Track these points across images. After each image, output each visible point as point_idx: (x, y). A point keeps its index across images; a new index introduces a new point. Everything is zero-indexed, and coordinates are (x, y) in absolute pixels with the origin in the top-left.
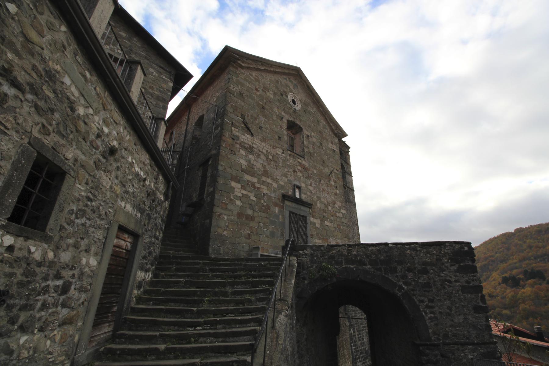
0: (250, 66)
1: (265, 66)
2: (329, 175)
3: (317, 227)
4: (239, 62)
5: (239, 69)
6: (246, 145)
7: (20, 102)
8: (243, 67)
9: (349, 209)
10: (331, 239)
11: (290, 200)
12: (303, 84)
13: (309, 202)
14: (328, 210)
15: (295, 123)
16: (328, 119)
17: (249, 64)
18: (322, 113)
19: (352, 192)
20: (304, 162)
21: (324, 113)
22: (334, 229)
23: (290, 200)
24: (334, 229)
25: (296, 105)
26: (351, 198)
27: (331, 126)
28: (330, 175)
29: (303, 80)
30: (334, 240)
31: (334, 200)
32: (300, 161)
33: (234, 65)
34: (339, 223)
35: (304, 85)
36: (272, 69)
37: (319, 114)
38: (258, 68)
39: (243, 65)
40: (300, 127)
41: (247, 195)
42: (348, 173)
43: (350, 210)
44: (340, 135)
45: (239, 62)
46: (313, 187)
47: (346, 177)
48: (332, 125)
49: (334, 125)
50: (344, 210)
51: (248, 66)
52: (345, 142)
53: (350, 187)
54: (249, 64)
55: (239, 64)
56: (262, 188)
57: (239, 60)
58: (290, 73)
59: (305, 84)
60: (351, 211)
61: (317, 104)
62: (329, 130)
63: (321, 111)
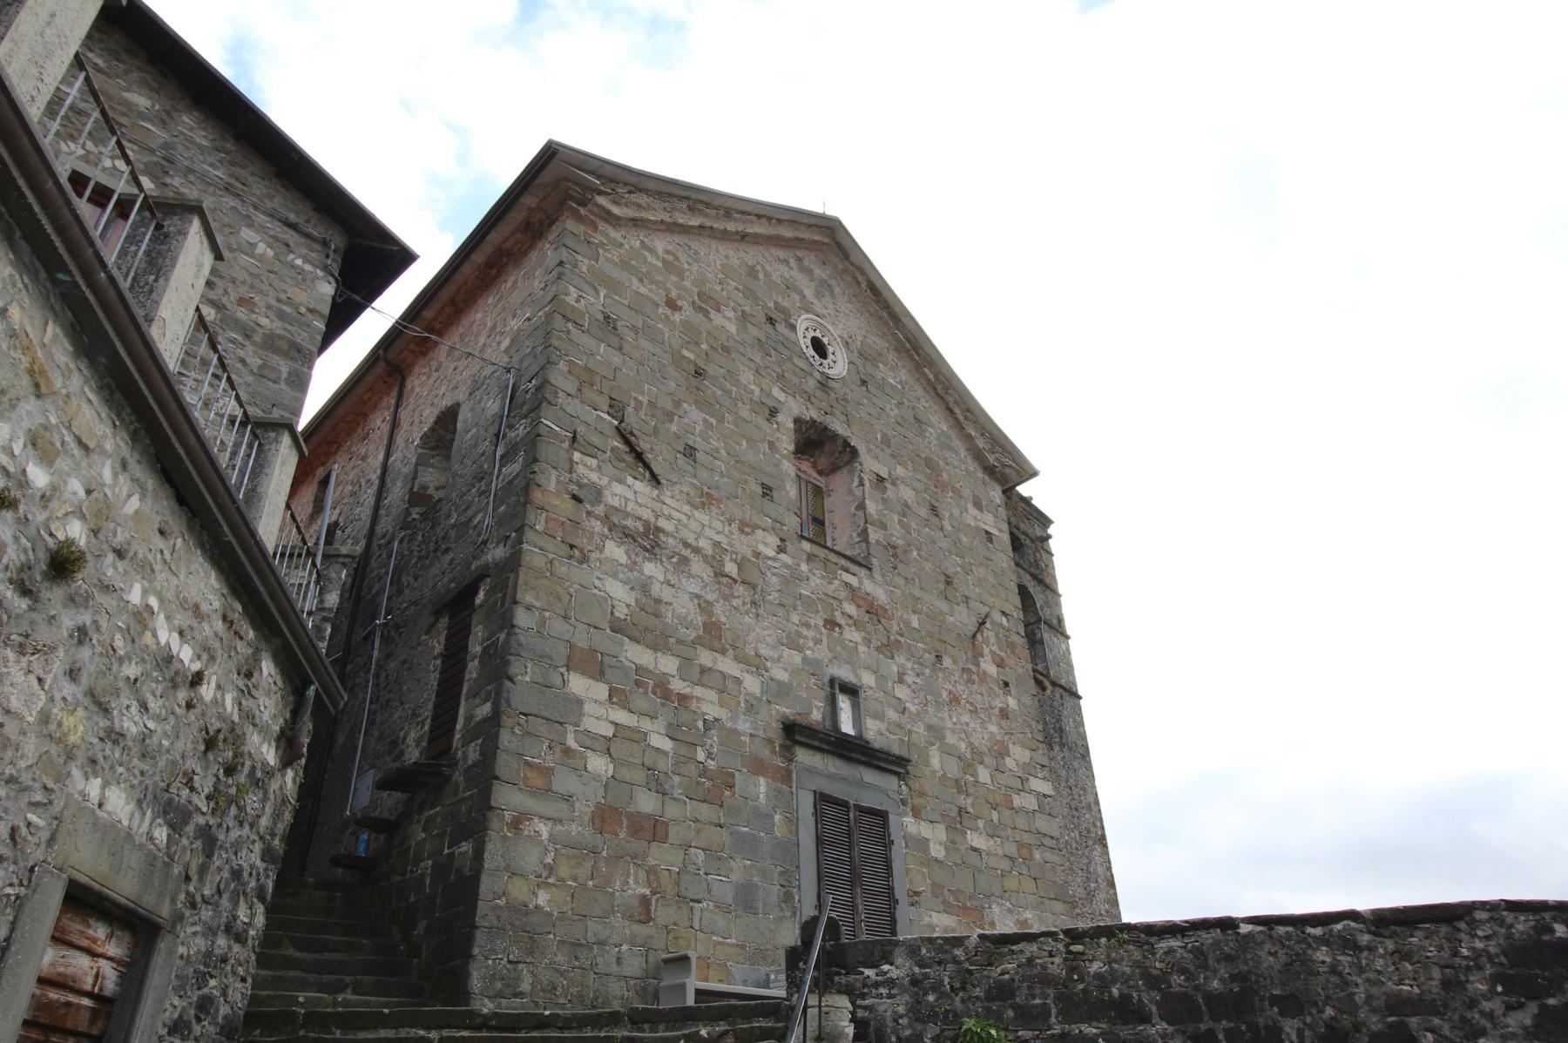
0: (644, 215)
2: (974, 636)
3: (936, 860)
4: (601, 200)
6: (629, 523)
8: (618, 218)
10: (996, 909)
11: (816, 744)
12: (855, 278)
16: (957, 411)
18: (935, 389)
21: (939, 388)
26: (1069, 725)
27: (969, 437)
29: (852, 264)
32: (853, 581)
33: (582, 211)
35: (859, 283)
37: (920, 392)
39: (616, 210)
40: (846, 444)
41: (636, 730)
42: (1050, 626)
44: (1007, 470)
45: (601, 200)
48: (973, 434)
49: (982, 435)
51: (637, 215)
57: (600, 193)
59: (860, 278)
60: (1072, 782)
62: (963, 453)
63: (929, 380)
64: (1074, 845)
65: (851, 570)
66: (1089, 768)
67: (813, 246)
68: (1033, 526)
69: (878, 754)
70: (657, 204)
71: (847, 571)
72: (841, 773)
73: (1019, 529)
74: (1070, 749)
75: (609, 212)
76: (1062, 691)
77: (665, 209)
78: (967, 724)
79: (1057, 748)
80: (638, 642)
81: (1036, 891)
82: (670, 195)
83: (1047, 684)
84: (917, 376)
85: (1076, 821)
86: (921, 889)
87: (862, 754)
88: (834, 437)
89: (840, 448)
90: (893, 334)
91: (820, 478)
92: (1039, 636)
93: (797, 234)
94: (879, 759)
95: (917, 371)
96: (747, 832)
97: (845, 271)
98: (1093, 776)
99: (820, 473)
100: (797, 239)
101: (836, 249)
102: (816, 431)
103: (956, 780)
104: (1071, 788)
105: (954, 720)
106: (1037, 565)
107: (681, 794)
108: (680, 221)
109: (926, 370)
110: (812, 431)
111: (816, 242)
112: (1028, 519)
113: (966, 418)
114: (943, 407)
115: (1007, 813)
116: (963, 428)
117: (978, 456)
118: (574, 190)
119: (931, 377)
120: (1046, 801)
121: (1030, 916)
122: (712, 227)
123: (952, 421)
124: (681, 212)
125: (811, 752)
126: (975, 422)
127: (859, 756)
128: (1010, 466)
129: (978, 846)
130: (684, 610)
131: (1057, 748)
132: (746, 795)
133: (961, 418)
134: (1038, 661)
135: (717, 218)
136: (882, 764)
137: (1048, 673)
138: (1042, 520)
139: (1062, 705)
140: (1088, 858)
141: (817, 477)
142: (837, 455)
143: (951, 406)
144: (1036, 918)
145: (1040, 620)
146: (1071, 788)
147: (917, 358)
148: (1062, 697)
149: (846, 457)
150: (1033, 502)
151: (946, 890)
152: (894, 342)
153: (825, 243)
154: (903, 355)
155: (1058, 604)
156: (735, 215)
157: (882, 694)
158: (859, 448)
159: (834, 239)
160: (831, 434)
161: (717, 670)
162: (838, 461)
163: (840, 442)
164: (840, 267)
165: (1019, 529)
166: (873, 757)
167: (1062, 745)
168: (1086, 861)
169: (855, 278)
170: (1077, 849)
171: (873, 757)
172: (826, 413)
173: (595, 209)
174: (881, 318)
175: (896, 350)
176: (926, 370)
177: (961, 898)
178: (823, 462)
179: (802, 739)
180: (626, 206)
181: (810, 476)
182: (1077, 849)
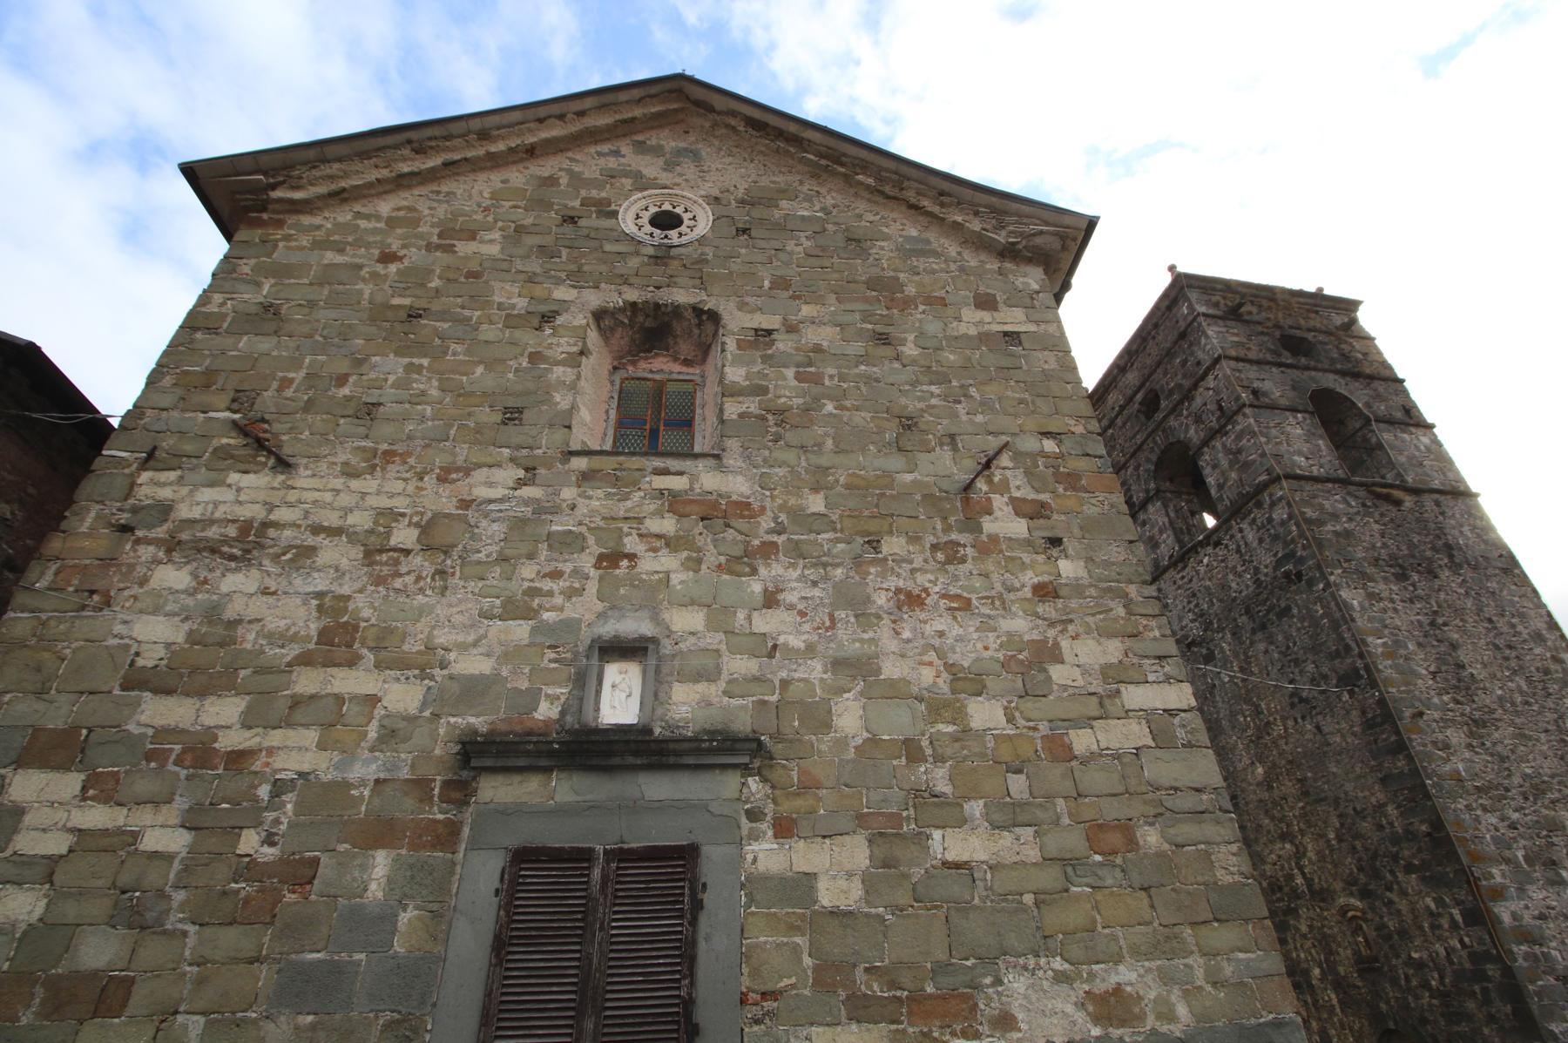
0: (343, 184)
1: (437, 150)
2: (968, 487)
3: (834, 913)
4: (278, 194)
5: (291, 219)
6: (213, 533)
7: (1132, 538)
8: (306, 202)
9: (1469, 603)
10: (1017, 984)
11: (521, 762)
12: (727, 126)
13: (743, 724)
14: (966, 730)
15: (657, 306)
16: (925, 203)
17: (332, 178)
18: (882, 193)
19: (1455, 508)
20: (709, 480)
21: (887, 189)
22: (1049, 878)
23: (521, 762)
24: (1049, 878)
25: (686, 222)
26: (1464, 537)
27: (957, 226)
28: (981, 485)
29: (719, 113)
30: (1060, 978)
31: (1035, 636)
32: (677, 483)
33: (265, 216)
34: (1113, 810)
35: (734, 129)
36: (500, 147)
37: (861, 206)
38: (402, 176)
39: (298, 195)
40: (697, 311)
41: (120, 832)
42: (1390, 422)
43: (1480, 611)
44: (1038, 241)
45: (278, 194)
46: (791, 607)
47: (1380, 446)
48: (959, 219)
49: (976, 214)
50: (1168, 679)
51: (333, 187)
52: (1320, 289)
53: (1436, 484)
54: (332, 178)
55: (280, 201)
56: (271, 751)
57: (274, 187)
58: (633, 120)
59: (733, 122)
60: (1490, 611)
61: (835, 174)
62: (952, 250)
63: (868, 187)
64: (1519, 700)
65: (672, 469)
66: (1523, 581)
67: (658, 121)
68: (1328, 318)
69: (671, 746)
70: (357, 166)
71: (665, 472)
72: (589, 797)
73: (1299, 328)
74: (1475, 568)
75: (291, 202)
76: (1436, 496)
77: (376, 167)
78: (941, 634)
79: (1445, 574)
80: (169, 692)
81: (1147, 913)
82: (379, 149)
83: (1397, 494)
84: (852, 191)
85: (1513, 664)
86: (786, 982)
87: (636, 754)
88: (677, 310)
89: (695, 321)
90: (802, 160)
91: (691, 370)
92: (1374, 440)
93: (618, 117)
94: (678, 754)
95: (851, 186)
96: (320, 961)
97: (715, 125)
98: (1535, 592)
99: (687, 362)
100: (624, 122)
101: (694, 108)
102: (647, 316)
103: (906, 742)
104: (1490, 621)
105: (906, 634)
106: (1345, 357)
107: (181, 921)
108: (406, 169)
109: (860, 177)
110: (641, 318)
111: (660, 115)
112: (1317, 312)
113: (942, 205)
114: (904, 208)
115: (1054, 774)
116: (943, 219)
117: (980, 243)
118: (246, 200)
119: (870, 181)
120: (1176, 721)
121: (1133, 976)
122: (466, 159)
123: (923, 220)
124: (404, 159)
125: (517, 778)
126: (959, 203)
127: (631, 760)
128: (1041, 232)
129: (965, 858)
130: (283, 623)
131: (1445, 574)
132: (333, 891)
133: (936, 209)
134: (1384, 471)
135: (470, 145)
136: (690, 760)
137: (1403, 481)
138: (1342, 306)
139: (1442, 513)
140: (1556, 712)
141: (684, 369)
142: (696, 331)
143: (913, 200)
144: (1149, 979)
145: (1368, 421)
146: (1490, 621)
147: (842, 170)
148: (1438, 504)
149: (709, 327)
150: (1326, 292)
151: (860, 975)
152: (806, 169)
153: (676, 110)
154: (825, 176)
155: (1405, 393)
156: (495, 133)
157: (721, 636)
158: (721, 310)
159: (688, 98)
160: (669, 309)
161: (328, 695)
162: (704, 339)
163: (689, 314)
164: (707, 125)
165: (1299, 328)
166: (661, 753)
167: (1455, 567)
168: (1550, 716)
169: (727, 126)
170: (1527, 703)
171: (661, 753)
172: (658, 288)
173: (277, 206)
174: (777, 151)
175: (814, 176)
176: (860, 177)
177: (906, 978)
178: (685, 348)
179: (489, 763)
180: (312, 185)
181: (671, 373)
182: (1527, 703)
